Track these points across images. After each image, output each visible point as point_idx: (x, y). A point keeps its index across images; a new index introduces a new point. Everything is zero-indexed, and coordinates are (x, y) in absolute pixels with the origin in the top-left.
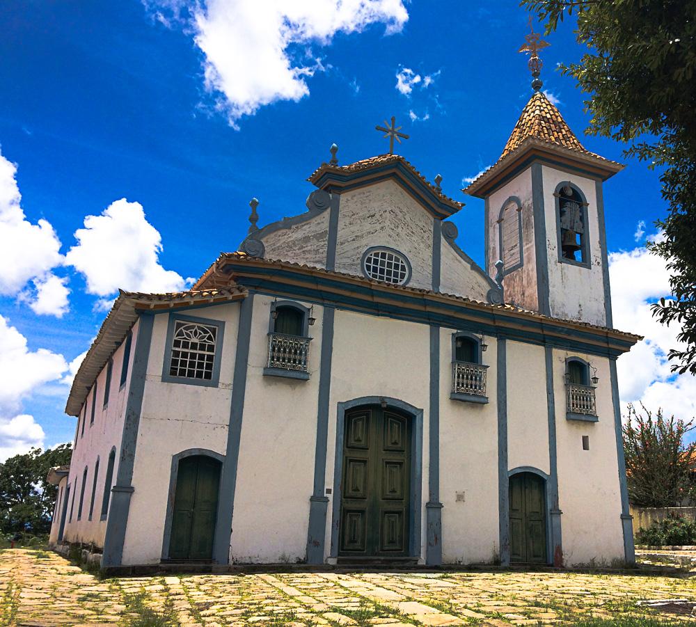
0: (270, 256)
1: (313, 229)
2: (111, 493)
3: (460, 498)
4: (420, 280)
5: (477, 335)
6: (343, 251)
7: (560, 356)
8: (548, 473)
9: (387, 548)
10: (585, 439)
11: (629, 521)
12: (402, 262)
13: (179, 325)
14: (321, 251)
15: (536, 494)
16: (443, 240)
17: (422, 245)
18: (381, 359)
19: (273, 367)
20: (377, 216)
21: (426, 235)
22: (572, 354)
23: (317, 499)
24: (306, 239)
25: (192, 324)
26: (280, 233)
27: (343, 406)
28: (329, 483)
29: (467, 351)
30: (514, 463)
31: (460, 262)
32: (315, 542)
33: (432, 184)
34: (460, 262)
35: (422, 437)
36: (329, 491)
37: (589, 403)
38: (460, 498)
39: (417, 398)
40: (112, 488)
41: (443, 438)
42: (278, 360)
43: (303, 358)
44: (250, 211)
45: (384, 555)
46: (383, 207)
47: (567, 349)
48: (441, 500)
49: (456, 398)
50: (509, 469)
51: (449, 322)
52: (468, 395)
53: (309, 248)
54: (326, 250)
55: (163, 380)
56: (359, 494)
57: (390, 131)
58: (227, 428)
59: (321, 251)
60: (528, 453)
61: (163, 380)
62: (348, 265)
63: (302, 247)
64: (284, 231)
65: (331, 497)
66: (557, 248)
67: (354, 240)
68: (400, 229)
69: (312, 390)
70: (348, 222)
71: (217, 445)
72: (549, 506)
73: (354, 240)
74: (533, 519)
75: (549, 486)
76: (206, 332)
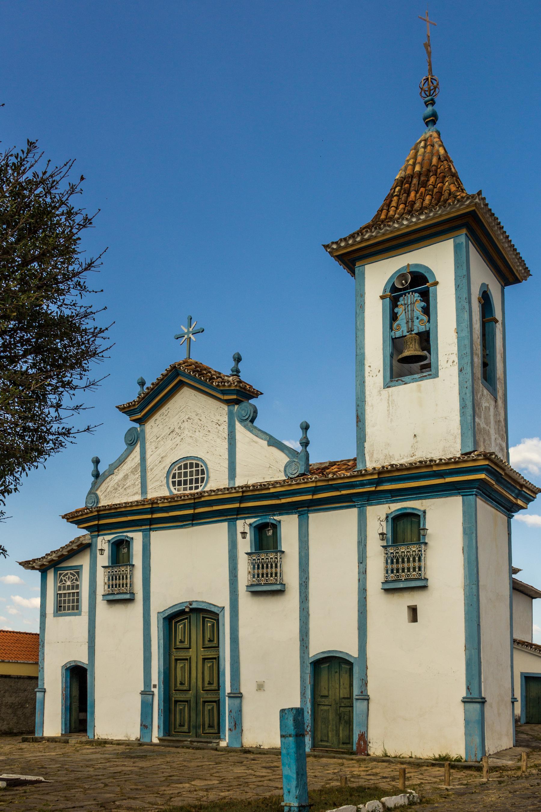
0: (103, 503)
1: (129, 466)
2: (227, 698)
3: (260, 687)
4: (217, 480)
5: (275, 518)
6: (153, 476)
7: (378, 515)
8: (356, 655)
9: (207, 731)
10: (413, 612)
11: (237, 701)
12: (176, 470)
13: (60, 574)
14: (137, 483)
15: (345, 677)
16: (239, 426)
17: (218, 441)
18: (190, 565)
19: (386, 582)
20: (177, 430)
21: (220, 428)
22: (395, 507)
23: (146, 693)
24: (126, 477)
25: (66, 572)
26: (108, 480)
27: (162, 614)
28: (155, 679)
29: (266, 540)
30: (316, 649)
31: (256, 443)
32: (144, 726)
33: (226, 370)
34: (256, 443)
35: (224, 633)
36: (155, 686)
37: (111, 582)
38: (260, 687)
39: (220, 599)
40: (227, 694)
41: (242, 633)
42: (414, 570)
43: (389, 566)
44: (92, 467)
45: (204, 738)
46: (181, 418)
47: (387, 502)
48: (242, 691)
49: (390, 589)
50: (310, 656)
51: (240, 513)
52: (267, 586)
53: (128, 484)
54: (140, 481)
55: (54, 616)
56: (186, 687)
57: (188, 336)
58: (87, 644)
59: (137, 483)
60: (333, 635)
61: (54, 616)
62: (159, 489)
63: (124, 485)
64: (110, 477)
65: (156, 691)
66: (382, 372)
67: (160, 462)
68: (197, 433)
69: (138, 606)
70: (153, 447)
71: (83, 659)
72: (356, 691)
73: (160, 462)
74: (343, 705)
75: (356, 669)
76: (74, 576)
